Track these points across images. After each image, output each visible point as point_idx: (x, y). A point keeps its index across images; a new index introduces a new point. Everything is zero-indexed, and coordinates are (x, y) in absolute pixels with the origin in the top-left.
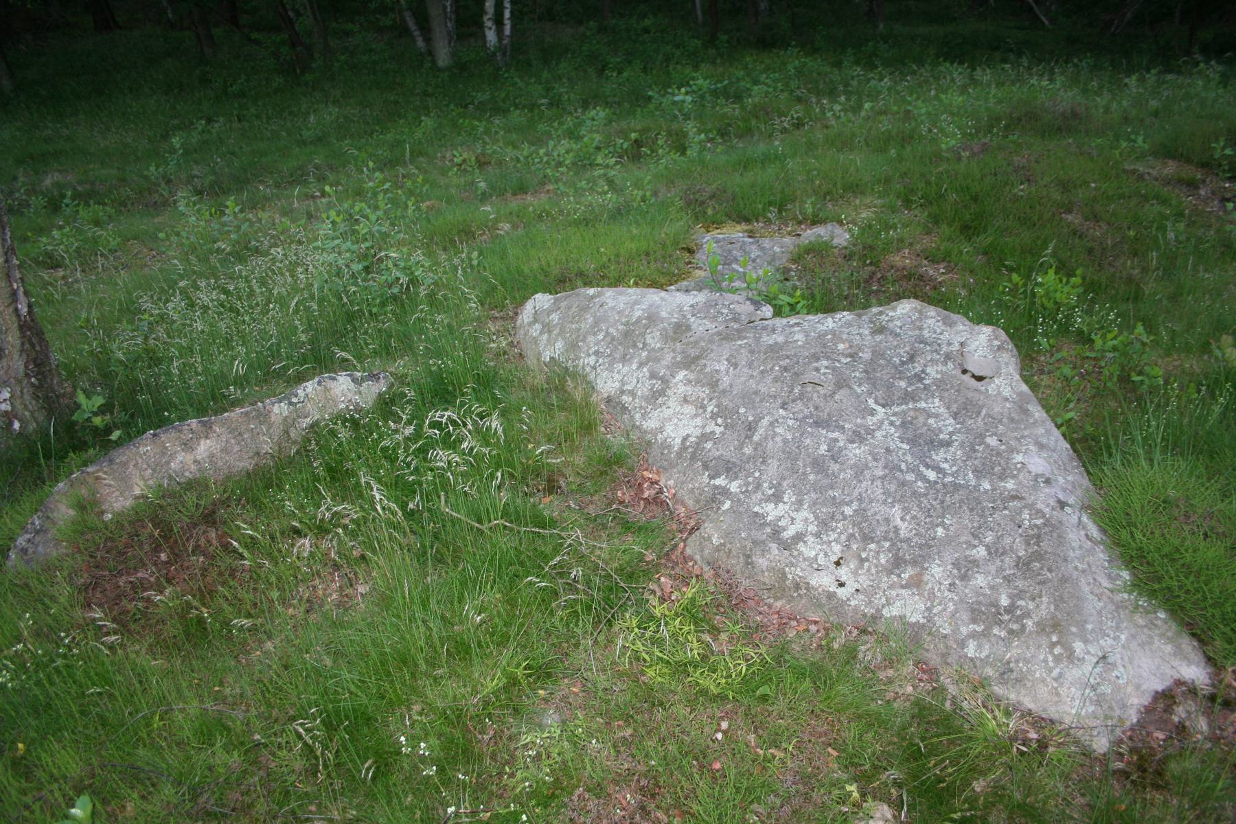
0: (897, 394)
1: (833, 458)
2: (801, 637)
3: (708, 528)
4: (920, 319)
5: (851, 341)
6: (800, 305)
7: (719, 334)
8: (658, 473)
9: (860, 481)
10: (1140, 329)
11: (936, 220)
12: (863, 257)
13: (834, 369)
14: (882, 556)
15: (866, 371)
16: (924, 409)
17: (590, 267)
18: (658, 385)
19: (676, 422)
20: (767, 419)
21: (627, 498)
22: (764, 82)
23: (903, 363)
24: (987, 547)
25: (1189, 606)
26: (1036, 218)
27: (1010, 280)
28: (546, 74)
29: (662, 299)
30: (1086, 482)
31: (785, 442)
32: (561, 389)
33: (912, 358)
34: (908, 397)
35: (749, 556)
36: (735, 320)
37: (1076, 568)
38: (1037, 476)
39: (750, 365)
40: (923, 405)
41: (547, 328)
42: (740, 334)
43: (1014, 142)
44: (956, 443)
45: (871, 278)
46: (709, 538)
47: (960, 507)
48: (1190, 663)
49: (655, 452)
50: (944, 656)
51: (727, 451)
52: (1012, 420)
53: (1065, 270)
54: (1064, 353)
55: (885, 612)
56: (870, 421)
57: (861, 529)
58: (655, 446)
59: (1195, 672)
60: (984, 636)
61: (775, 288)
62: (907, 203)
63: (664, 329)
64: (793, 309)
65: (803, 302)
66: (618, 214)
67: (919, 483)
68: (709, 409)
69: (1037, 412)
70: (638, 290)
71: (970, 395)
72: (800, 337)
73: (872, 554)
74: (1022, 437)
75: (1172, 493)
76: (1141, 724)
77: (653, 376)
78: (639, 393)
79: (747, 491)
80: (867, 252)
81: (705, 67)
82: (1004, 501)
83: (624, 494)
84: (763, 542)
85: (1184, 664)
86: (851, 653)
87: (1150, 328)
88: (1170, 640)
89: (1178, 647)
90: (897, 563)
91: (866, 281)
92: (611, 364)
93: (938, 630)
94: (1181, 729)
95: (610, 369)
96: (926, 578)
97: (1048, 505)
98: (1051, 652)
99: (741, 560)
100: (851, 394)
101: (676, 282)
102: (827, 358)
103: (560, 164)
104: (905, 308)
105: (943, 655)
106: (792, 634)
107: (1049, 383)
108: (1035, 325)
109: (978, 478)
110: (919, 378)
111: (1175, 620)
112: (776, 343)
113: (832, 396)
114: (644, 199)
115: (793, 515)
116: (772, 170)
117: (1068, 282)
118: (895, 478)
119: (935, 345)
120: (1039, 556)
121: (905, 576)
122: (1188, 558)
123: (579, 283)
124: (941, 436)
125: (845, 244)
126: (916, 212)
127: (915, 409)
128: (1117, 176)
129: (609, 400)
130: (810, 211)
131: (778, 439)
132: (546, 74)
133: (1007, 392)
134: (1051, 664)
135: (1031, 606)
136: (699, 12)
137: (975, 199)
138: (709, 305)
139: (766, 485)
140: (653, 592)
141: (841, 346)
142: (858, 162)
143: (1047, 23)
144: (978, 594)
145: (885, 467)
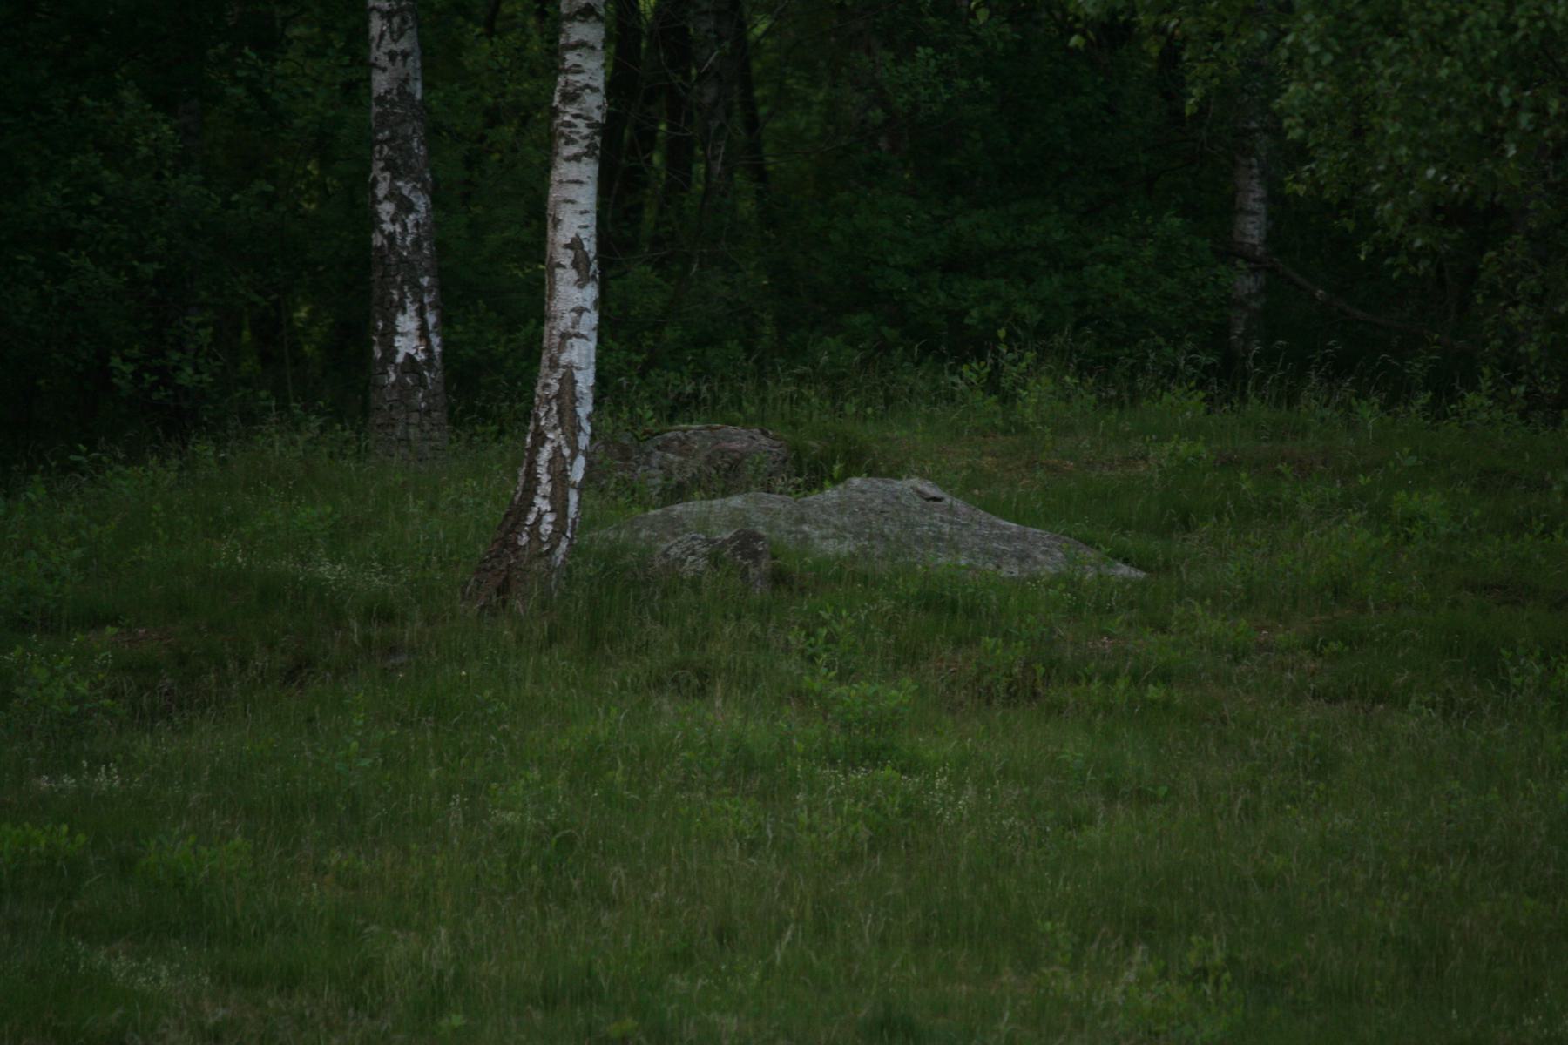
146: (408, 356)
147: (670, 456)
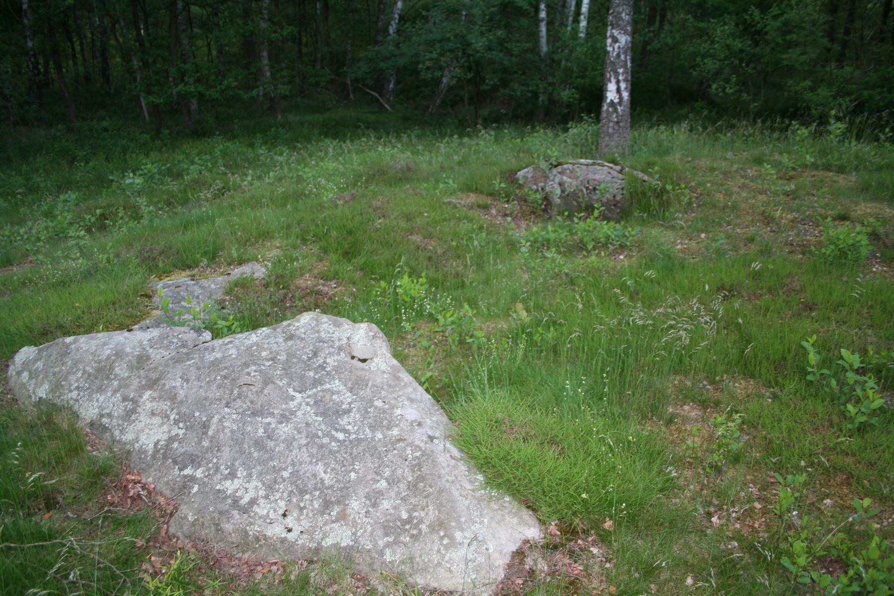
0: (309, 382)
1: (269, 437)
2: (266, 578)
3: (184, 509)
4: (317, 325)
5: (270, 349)
6: (234, 327)
7: (172, 358)
8: (139, 474)
9: (291, 451)
10: (466, 306)
11: (325, 251)
12: (277, 284)
13: (260, 371)
14: (315, 502)
15: (284, 369)
16: (329, 390)
17: (67, 319)
18: (130, 406)
19: (148, 432)
20: (216, 417)
21: (116, 500)
22: (197, 162)
23: (310, 359)
24: (387, 480)
25: (522, 489)
26: (392, 241)
27: (379, 287)
28: (24, 168)
29: (125, 338)
30: (445, 419)
31: (232, 432)
32: (49, 422)
33: (315, 354)
34: (316, 382)
35: (218, 525)
36: (183, 346)
37: (447, 481)
38: (412, 422)
39: (198, 379)
40: (328, 386)
41: (33, 375)
42: (188, 357)
43: (373, 191)
44: (354, 410)
45: (285, 298)
46: (186, 517)
47: (364, 455)
48: (530, 527)
49: (134, 458)
50: (370, 565)
51: (190, 447)
52: (390, 386)
53: (414, 273)
54: (422, 331)
55: (323, 543)
56: (292, 405)
57: (297, 486)
58: (134, 454)
59: (533, 532)
60: (395, 544)
61: (214, 316)
62: (304, 241)
63: (130, 361)
64: (230, 330)
65: (236, 324)
66: (88, 275)
67: (333, 444)
68: (172, 417)
69: (406, 377)
70: (106, 334)
71: (359, 373)
72: (233, 352)
73: (308, 502)
74: (399, 396)
75: (500, 416)
76: (507, 577)
77: (125, 399)
78: (116, 414)
79: (209, 475)
80: (280, 280)
81: (153, 155)
82: (393, 444)
83: (113, 497)
84: (227, 511)
85: (526, 528)
86: (304, 581)
87: (473, 303)
88: (515, 514)
89: (521, 518)
90: (327, 505)
91: (282, 301)
92: (90, 395)
93: (363, 548)
94: (532, 572)
95: (90, 399)
96: (348, 511)
97: (422, 441)
98: (441, 544)
99: (213, 528)
100: (276, 388)
101: (139, 322)
102: (255, 364)
103: (39, 239)
104: (306, 318)
105: (370, 565)
106: (259, 576)
107: (415, 352)
108: (401, 314)
109: (373, 432)
110: (322, 367)
111: (516, 500)
112: (216, 359)
113: (262, 392)
114: (108, 261)
115: (247, 485)
116: (204, 228)
117: (418, 282)
118: (315, 443)
119: (330, 342)
120: (422, 478)
121: (334, 513)
122: (516, 457)
123: (59, 334)
124: (344, 407)
125: (263, 276)
126: (311, 247)
127: (323, 391)
128: (440, 207)
129: (92, 424)
130: (235, 255)
131: (227, 431)
132: (24, 168)
133: (383, 367)
134: (443, 552)
135: (423, 514)
136: (146, 114)
137: (350, 233)
138: (162, 338)
139: (222, 467)
140: (146, 571)
141: (264, 354)
142: (268, 216)
143: (389, 108)
144: (386, 515)
145: (307, 437)
146: (612, 101)
147: (565, 178)
